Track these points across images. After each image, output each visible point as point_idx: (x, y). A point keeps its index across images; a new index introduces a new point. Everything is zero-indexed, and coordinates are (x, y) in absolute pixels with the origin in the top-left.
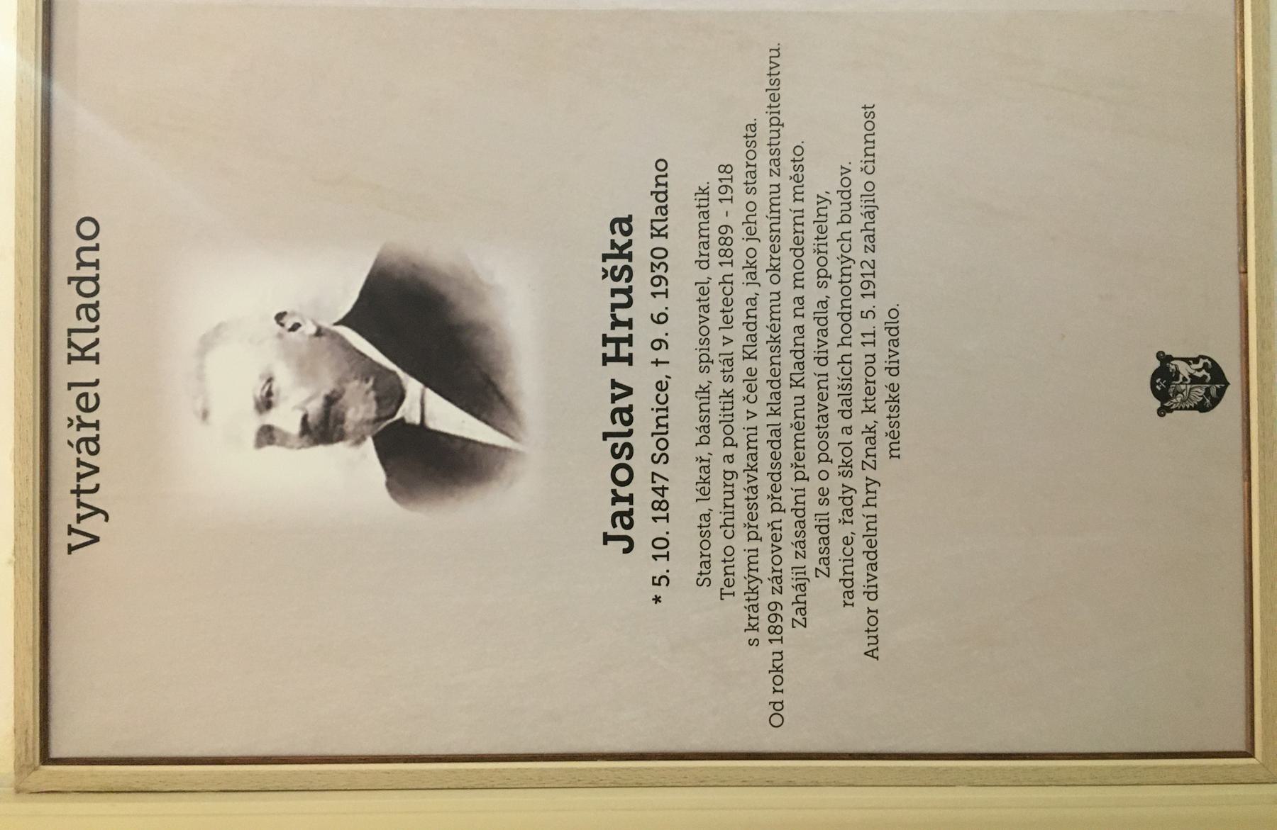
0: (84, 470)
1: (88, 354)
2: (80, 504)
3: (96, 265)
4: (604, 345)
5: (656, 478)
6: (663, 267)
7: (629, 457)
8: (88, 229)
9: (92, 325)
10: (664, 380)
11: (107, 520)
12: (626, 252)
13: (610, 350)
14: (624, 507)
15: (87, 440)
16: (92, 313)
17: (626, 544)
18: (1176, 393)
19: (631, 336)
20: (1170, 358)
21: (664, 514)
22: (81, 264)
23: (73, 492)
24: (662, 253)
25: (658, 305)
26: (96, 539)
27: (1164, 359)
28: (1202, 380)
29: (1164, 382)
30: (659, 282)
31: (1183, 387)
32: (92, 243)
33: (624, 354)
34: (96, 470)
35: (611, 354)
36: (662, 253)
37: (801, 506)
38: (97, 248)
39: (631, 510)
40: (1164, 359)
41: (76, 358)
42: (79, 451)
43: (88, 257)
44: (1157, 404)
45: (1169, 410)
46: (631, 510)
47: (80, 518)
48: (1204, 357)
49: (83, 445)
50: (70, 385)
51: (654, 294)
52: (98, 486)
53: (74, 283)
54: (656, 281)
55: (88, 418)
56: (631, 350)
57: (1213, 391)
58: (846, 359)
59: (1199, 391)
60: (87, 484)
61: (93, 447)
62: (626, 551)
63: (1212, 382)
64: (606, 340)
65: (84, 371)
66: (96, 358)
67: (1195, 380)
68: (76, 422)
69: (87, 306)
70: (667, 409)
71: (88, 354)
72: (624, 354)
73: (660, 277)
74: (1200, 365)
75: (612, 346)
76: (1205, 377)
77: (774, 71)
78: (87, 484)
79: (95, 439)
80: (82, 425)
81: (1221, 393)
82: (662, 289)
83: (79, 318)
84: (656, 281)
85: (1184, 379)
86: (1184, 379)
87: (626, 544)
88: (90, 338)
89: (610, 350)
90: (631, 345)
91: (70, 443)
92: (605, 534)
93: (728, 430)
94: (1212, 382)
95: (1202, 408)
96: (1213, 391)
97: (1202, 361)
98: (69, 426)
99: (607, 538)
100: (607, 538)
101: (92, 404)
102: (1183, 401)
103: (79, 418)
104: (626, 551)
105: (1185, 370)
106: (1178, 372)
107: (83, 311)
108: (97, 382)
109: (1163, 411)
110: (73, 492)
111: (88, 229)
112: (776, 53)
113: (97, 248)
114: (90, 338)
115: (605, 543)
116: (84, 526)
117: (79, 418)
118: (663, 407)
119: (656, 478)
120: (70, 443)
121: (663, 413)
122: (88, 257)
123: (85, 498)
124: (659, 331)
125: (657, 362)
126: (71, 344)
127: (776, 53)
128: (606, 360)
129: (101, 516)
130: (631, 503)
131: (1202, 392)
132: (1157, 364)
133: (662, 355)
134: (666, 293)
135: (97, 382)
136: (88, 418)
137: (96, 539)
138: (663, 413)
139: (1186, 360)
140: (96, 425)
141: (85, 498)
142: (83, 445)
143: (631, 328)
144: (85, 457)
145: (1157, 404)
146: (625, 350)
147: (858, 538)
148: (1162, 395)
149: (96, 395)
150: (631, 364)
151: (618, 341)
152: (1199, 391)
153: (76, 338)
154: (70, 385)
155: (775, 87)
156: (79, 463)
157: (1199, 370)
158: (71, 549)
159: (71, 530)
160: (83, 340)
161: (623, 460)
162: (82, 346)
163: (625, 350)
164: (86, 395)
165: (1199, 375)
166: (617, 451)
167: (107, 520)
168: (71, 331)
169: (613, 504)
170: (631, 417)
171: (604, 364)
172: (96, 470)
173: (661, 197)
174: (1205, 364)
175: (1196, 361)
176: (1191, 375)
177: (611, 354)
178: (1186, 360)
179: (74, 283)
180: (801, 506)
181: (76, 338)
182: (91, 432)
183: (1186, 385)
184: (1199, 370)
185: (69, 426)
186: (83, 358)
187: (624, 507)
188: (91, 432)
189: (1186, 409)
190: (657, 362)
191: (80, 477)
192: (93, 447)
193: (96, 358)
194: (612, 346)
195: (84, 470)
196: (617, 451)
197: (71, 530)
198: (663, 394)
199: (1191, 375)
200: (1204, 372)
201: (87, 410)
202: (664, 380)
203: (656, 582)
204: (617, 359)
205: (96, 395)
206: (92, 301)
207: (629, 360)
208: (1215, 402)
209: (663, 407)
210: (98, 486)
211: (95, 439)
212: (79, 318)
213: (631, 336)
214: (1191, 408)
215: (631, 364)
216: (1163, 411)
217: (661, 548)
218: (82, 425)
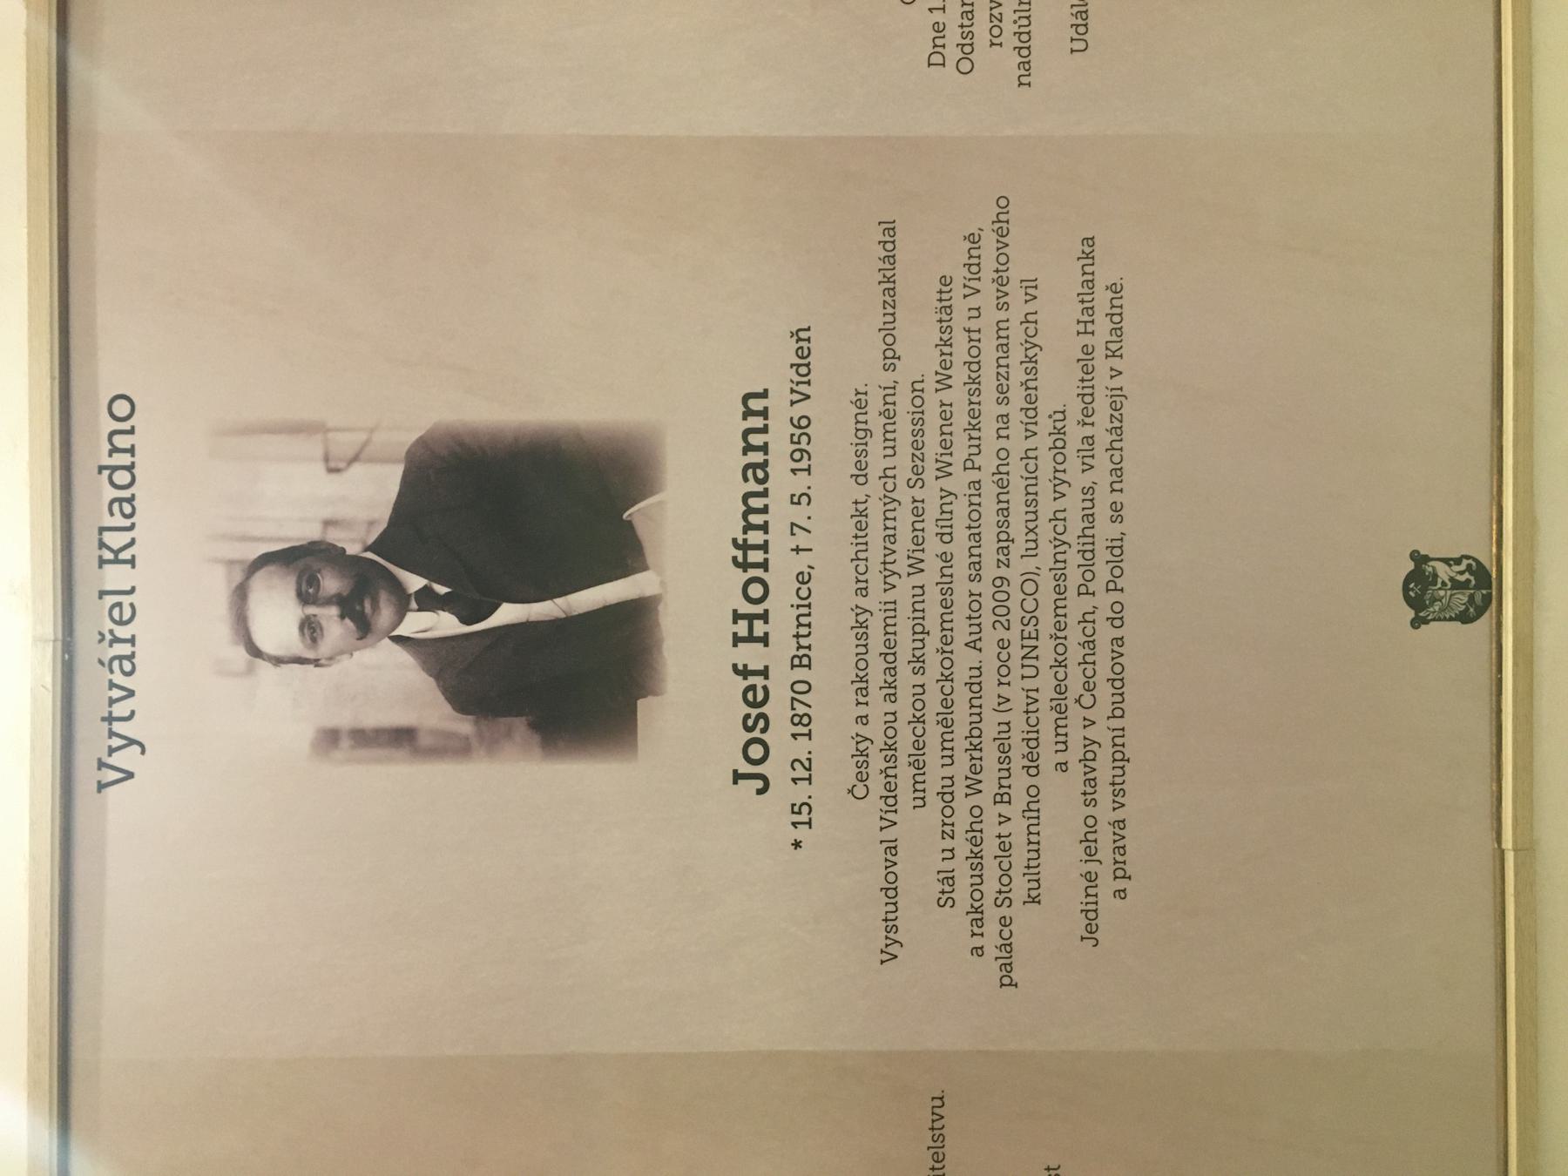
0: (116, 693)
1: (122, 556)
2: (112, 734)
3: (131, 451)
4: (735, 622)
5: (796, 704)
6: (804, 438)
7: (764, 730)
8: (122, 408)
9: (127, 523)
10: (807, 570)
11: (143, 752)
12: (125, 555)
13: (742, 628)
14: (757, 457)
15: (121, 658)
16: (127, 509)
17: (759, 784)
18: (1434, 600)
19: (766, 542)
20: (1426, 559)
21: (805, 730)
22: (114, 450)
23: (103, 719)
24: (804, 687)
25: (800, 483)
26: (130, 775)
27: (1419, 559)
28: (1464, 585)
29: (1419, 589)
30: (802, 722)
31: (1442, 593)
32: (126, 426)
33: (758, 632)
34: (131, 693)
35: (743, 632)
36: (804, 687)
37: (975, 261)
38: (132, 431)
39: (766, 461)
40: (1419, 559)
41: (109, 562)
42: (112, 672)
43: (122, 441)
44: (1411, 614)
45: (1426, 621)
46: (766, 461)
47: (111, 751)
48: (1468, 557)
49: (116, 664)
50: (102, 594)
51: (794, 471)
52: (133, 713)
53: (106, 473)
54: (797, 455)
55: (122, 632)
56: (766, 628)
57: (1478, 598)
58: (1030, 318)
59: (1462, 598)
60: (120, 710)
61: (127, 666)
62: (760, 792)
63: (1477, 587)
64: (737, 616)
65: (116, 577)
66: (132, 562)
67: (1457, 585)
68: (108, 637)
69: (120, 500)
70: (809, 606)
71: (122, 556)
72: (758, 632)
73: (801, 450)
74: (1463, 567)
75: (743, 624)
76: (1468, 581)
77: (937, 1125)
78: (120, 710)
79: (131, 657)
80: (116, 640)
81: (1487, 600)
82: (804, 464)
83: (112, 514)
84: (797, 455)
85: (1444, 583)
86: (1444, 583)
87: (759, 784)
88: (125, 538)
89: (742, 628)
90: (766, 622)
91: (101, 663)
92: (735, 772)
93: (889, 340)
94: (1477, 587)
95: (1464, 618)
96: (1478, 598)
97: (1465, 562)
98: (100, 641)
99: (737, 777)
100: (737, 777)
101: (127, 615)
102: (1441, 610)
103: (111, 632)
104: (760, 792)
105: (1443, 572)
106: (1435, 576)
107: (116, 506)
108: (133, 590)
109: (1417, 623)
110: (103, 719)
111: (122, 408)
112: (938, 1103)
113: (132, 431)
114: (125, 538)
115: (735, 782)
116: (115, 760)
117: (111, 632)
118: (804, 604)
119: (796, 704)
120: (101, 663)
121: (804, 610)
122: (122, 441)
123: (118, 727)
124: (799, 514)
125: (797, 550)
126: (102, 545)
127: (938, 1103)
128: (737, 640)
129: (137, 749)
130: (766, 552)
131: (1466, 599)
132: (1411, 566)
133: (802, 539)
134: (808, 470)
135: (133, 590)
136: (122, 632)
137: (130, 775)
138: (804, 610)
139: (1446, 561)
140: (132, 641)
141: (118, 727)
142: (116, 664)
143: (766, 532)
144: (118, 678)
145: (1411, 614)
146: (759, 628)
147: (1044, 572)
148: (1416, 603)
149: (132, 605)
150: (766, 645)
151: (750, 618)
152: (1462, 598)
153: (109, 538)
154: (102, 594)
155: (939, 1144)
156: (112, 685)
157: (1462, 573)
158: (101, 786)
159: (101, 765)
160: (115, 540)
161: (756, 734)
162: (115, 547)
163: (759, 628)
164: (119, 605)
165: (1462, 578)
166: (750, 723)
167: (143, 752)
168: (102, 530)
169: (745, 453)
170: (767, 476)
171: (735, 645)
172: (131, 693)
173: (803, 370)
174: (1469, 566)
175: (1458, 561)
176: (1452, 579)
177: (743, 632)
178: (1446, 561)
179: (106, 473)
180: (975, 261)
181: (109, 538)
182: (125, 649)
183: (1454, 590)
184: (1462, 573)
185: (100, 641)
186: (116, 561)
187: (757, 457)
188: (125, 649)
189: (1445, 619)
190: (797, 550)
191: (112, 702)
192: (127, 666)
193: (132, 562)
194: (743, 624)
195: (116, 693)
196: (750, 723)
197: (101, 765)
198: (804, 587)
199: (1452, 579)
200: (1467, 576)
201: (121, 623)
202: (807, 570)
203: (795, 809)
204: (751, 638)
205: (132, 605)
206: (126, 494)
207: (765, 640)
208: (1480, 612)
209: (804, 604)
210: (133, 713)
211: (131, 657)
212: (112, 514)
213: (766, 560)
214: (1451, 619)
215: (766, 645)
216: (1417, 623)
217: (804, 770)
218: (116, 640)
